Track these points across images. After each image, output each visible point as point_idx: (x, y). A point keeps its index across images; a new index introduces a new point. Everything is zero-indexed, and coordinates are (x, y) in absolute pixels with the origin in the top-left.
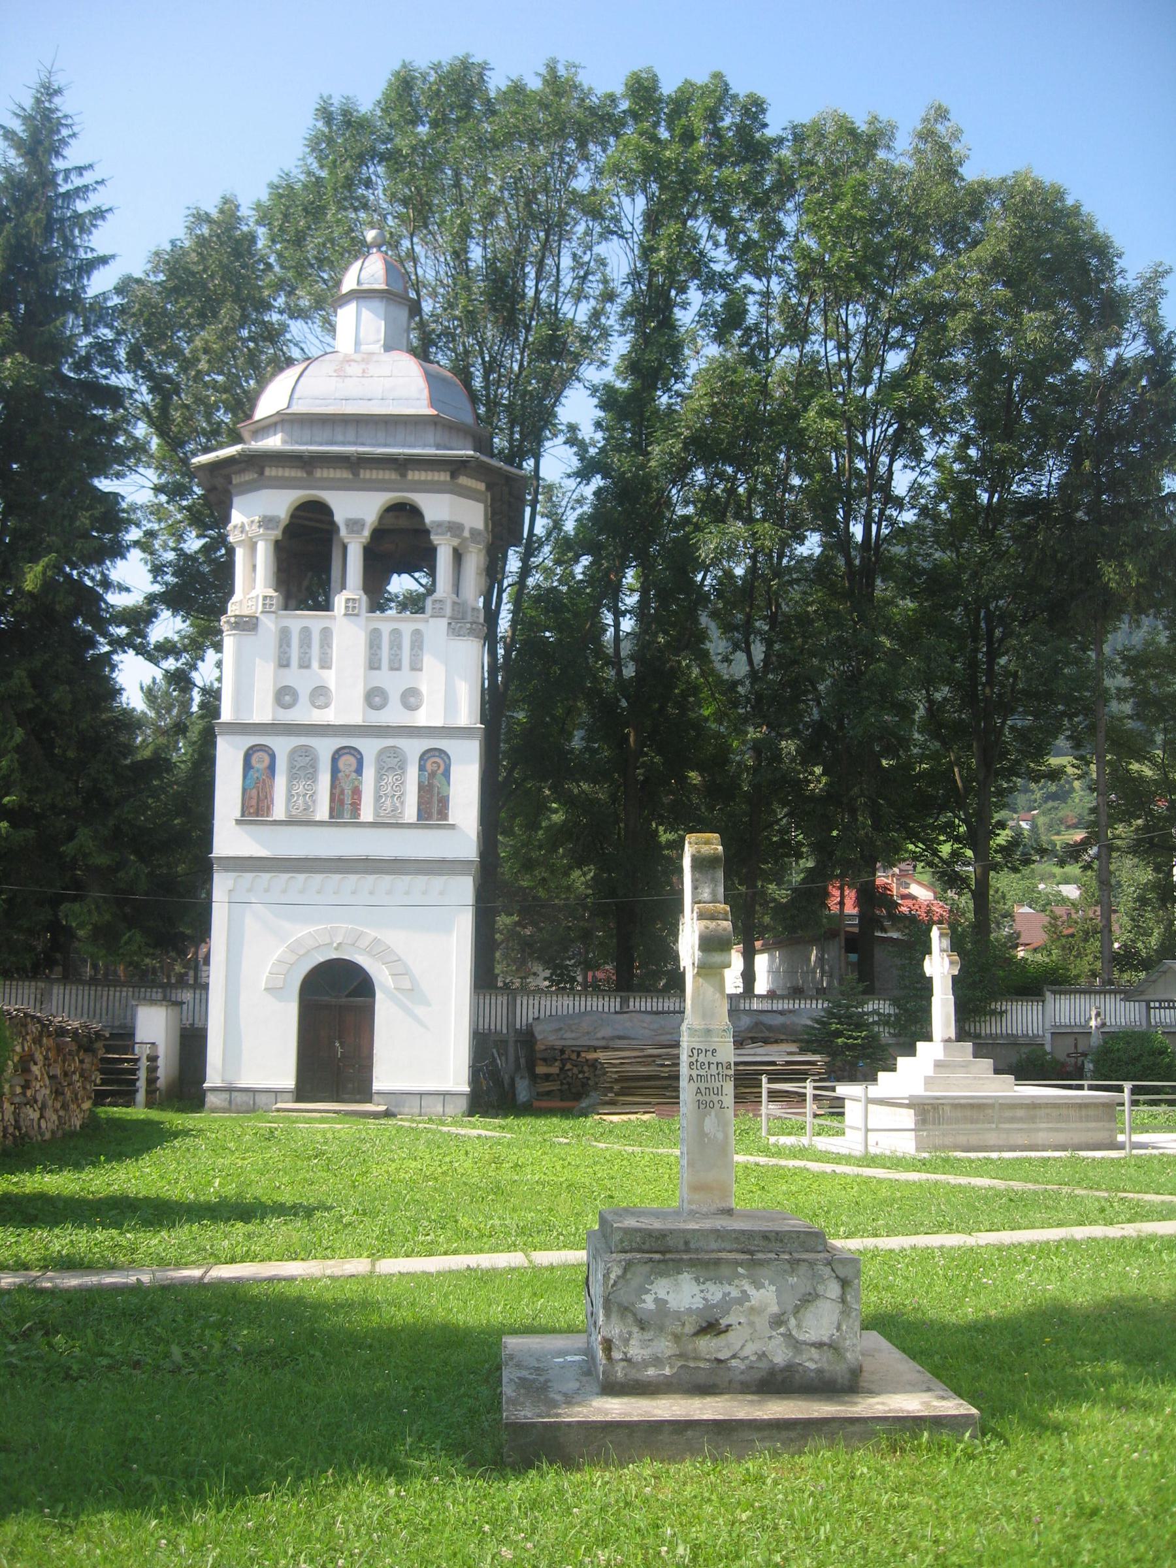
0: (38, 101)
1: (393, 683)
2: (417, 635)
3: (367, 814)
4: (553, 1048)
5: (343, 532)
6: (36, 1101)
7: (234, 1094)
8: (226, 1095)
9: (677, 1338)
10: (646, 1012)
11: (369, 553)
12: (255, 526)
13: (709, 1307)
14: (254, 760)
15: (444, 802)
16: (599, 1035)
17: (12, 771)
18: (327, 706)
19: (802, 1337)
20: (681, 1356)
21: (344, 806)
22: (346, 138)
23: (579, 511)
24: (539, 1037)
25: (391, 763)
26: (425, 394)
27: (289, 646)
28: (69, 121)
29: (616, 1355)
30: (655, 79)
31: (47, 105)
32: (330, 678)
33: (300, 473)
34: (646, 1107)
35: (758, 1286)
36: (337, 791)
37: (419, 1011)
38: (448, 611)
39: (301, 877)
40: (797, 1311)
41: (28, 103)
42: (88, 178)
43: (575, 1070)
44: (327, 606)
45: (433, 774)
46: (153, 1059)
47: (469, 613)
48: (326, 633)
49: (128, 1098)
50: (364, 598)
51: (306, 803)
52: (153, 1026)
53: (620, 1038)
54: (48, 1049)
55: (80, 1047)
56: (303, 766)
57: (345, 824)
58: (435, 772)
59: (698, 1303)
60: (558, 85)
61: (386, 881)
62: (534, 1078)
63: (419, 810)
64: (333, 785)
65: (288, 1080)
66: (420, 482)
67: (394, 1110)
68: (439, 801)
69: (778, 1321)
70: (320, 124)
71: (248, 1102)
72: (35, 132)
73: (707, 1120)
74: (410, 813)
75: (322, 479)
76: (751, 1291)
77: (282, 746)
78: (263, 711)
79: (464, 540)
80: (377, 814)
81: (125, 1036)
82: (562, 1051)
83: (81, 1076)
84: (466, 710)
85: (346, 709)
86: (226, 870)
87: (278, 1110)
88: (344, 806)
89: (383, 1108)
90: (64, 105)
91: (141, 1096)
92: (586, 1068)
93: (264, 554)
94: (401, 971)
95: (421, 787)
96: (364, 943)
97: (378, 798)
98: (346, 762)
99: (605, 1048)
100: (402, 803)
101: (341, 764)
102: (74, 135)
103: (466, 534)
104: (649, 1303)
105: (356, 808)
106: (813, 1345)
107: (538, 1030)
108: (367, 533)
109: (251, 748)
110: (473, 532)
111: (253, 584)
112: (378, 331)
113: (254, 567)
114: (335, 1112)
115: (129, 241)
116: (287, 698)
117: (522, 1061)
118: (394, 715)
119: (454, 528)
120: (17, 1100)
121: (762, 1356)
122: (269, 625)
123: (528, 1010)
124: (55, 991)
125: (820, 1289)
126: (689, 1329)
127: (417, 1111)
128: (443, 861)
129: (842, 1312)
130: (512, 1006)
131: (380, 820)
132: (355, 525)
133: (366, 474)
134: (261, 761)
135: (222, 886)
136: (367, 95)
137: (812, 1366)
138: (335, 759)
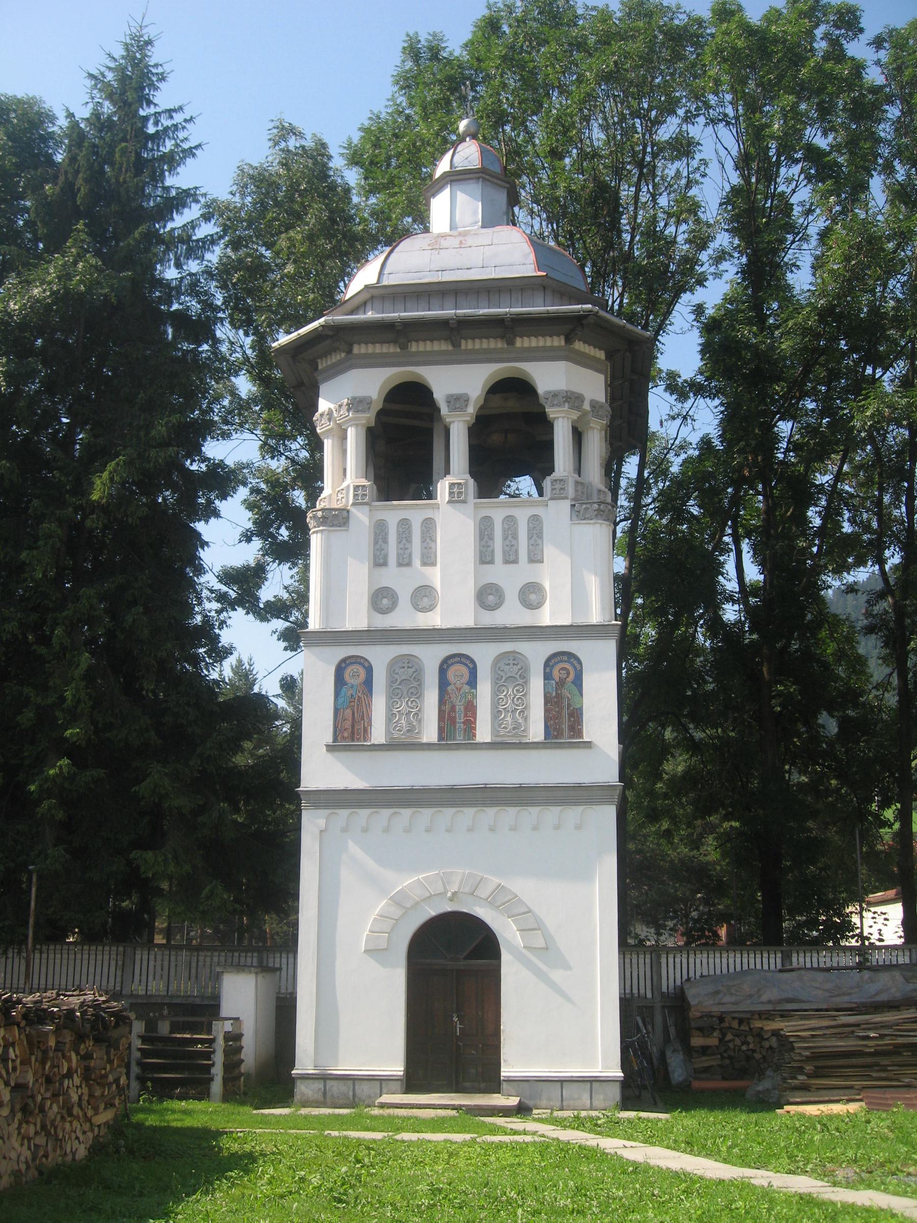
1: (509, 579)
2: (536, 524)
3: (484, 733)
4: (709, 1015)
5: (444, 410)
7: (330, 1083)
8: (319, 1085)
10: (812, 968)
12: (344, 411)
14: (347, 676)
15: (576, 717)
16: (764, 998)
17: (79, 701)
18: (431, 608)
21: (456, 727)
22: (436, 83)
23: (683, 456)
24: (693, 1002)
25: (511, 673)
26: (532, 257)
27: (385, 541)
32: (435, 576)
34: (848, 1094)
36: (447, 708)
37: (557, 975)
38: (571, 491)
39: (406, 813)
42: (178, 118)
43: (738, 1042)
44: (431, 496)
45: (561, 683)
46: (234, 1038)
47: (595, 493)
48: (429, 526)
49: (198, 1087)
50: (471, 482)
51: (409, 723)
52: (241, 997)
53: (789, 1001)
55: (80, 1038)
56: (406, 681)
57: (458, 747)
58: (564, 679)
61: (552, 813)
62: (689, 1051)
63: (546, 727)
64: (442, 701)
65: (397, 1068)
66: (530, 349)
67: (530, 1103)
68: (571, 715)
70: (409, 64)
71: (351, 1092)
72: (123, 79)
74: (536, 730)
75: (418, 353)
77: (380, 657)
79: (585, 414)
80: (495, 732)
81: (208, 1009)
82: (721, 1019)
84: (598, 607)
85: (455, 609)
86: (317, 806)
87: (382, 1106)
88: (456, 727)
89: (514, 1101)
90: (156, 56)
91: (217, 1086)
92: (750, 1039)
93: (354, 439)
94: (532, 925)
95: (547, 700)
96: (484, 892)
97: (496, 714)
98: (457, 676)
100: (526, 719)
103: (587, 406)
105: (470, 726)
107: (693, 995)
108: (471, 409)
109: (344, 661)
110: (594, 404)
111: (344, 472)
112: (475, 213)
113: (345, 470)
114: (454, 1107)
116: (385, 601)
117: (672, 1030)
118: (512, 614)
119: (572, 399)
122: (361, 517)
123: (674, 971)
124: (138, 957)
127: (558, 1104)
128: (579, 787)
130: (656, 967)
131: (499, 739)
134: (356, 675)
135: (312, 825)
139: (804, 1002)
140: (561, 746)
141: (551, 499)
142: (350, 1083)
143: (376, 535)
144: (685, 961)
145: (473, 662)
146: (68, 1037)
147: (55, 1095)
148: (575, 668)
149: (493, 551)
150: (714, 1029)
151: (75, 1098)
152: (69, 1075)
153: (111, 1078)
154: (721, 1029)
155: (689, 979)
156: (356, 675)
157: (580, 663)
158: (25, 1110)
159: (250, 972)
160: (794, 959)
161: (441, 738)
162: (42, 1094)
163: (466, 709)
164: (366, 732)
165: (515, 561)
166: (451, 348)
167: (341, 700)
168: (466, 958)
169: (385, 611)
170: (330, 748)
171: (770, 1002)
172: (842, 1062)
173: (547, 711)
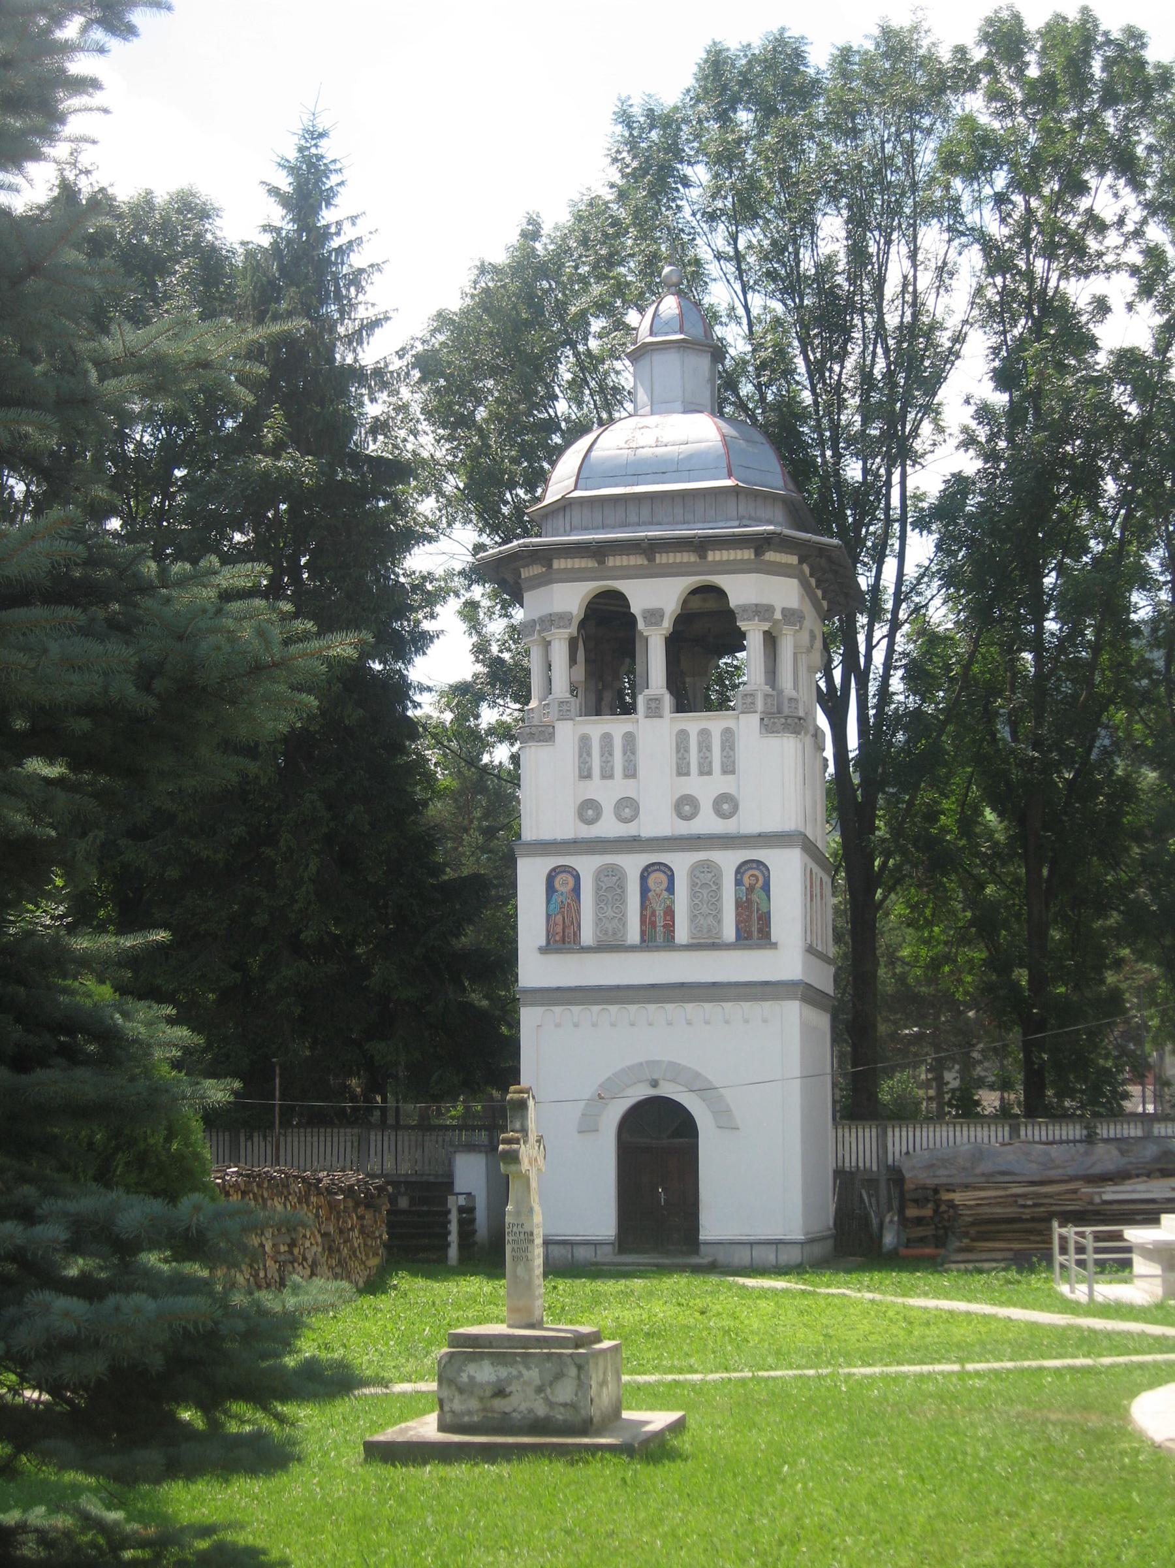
0: (301, 149)
4: (924, 1188)
5: (641, 625)
6: (305, 1259)
9: (481, 1399)
11: (674, 643)
13: (499, 1380)
15: (765, 920)
16: (978, 1171)
19: (553, 1399)
20: (484, 1410)
27: (589, 754)
28: (338, 166)
29: (446, 1408)
30: (1017, 19)
31: (313, 151)
33: (590, 563)
35: (528, 1368)
38: (760, 705)
40: (551, 1384)
41: (292, 155)
45: (751, 889)
46: (467, 1211)
52: (469, 1174)
54: (319, 1207)
55: (357, 1204)
58: (754, 886)
59: (493, 1378)
60: (896, 45)
61: (709, 1009)
64: (643, 906)
66: (721, 563)
68: (759, 919)
69: (540, 1390)
73: (519, 1269)
76: (524, 1371)
78: (567, 828)
79: (776, 622)
82: (936, 1191)
83: (362, 1232)
85: (657, 820)
86: (533, 1004)
91: (453, 1252)
95: (738, 904)
99: (967, 1187)
101: (651, 882)
102: (341, 184)
103: (778, 615)
104: (464, 1378)
105: (670, 928)
106: (561, 1405)
109: (554, 870)
115: (407, 294)
116: (590, 812)
119: (762, 611)
120: (282, 1258)
121: (531, 1411)
124: (372, 1137)
125: (565, 1371)
126: (488, 1393)
129: (579, 1385)
132: (654, 616)
133: (661, 558)
134: (565, 883)
135: (529, 1018)
136: (672, 83)
137: (560, 1417)
138: (644, 878)
139: (1015, 1174)
140: (750, 947)
141: (742, 713)
142: (569, 1247)
143: (580, 748)
144: (911, 1134)
145: (671, 870)
146: (350, 1204)
147: (345, 1242)
148: (764, 875)
149: (689, 763)
150: (928, 1201)
151: (356, 1245)
152: (352, 1229)
153: (377, 1234)
154: (935, 1201)
155: (908, 1153)
156: (565, 883)
157: (768, 869)
158: (330, 1249)
159: (480, 1152)
160: (1022, 1133)
161: (643, 940)
162: (339, 1240)
163: (665, 914)
164: (577, 935)
165: (710, 773)
166: (646, 562)
167: (552, 907)
168: (669, 1137)
169: (590, 822)
170: (544, 950)
171: (983, 1174)
172: (1003, 1227)
173: (737, 915)
